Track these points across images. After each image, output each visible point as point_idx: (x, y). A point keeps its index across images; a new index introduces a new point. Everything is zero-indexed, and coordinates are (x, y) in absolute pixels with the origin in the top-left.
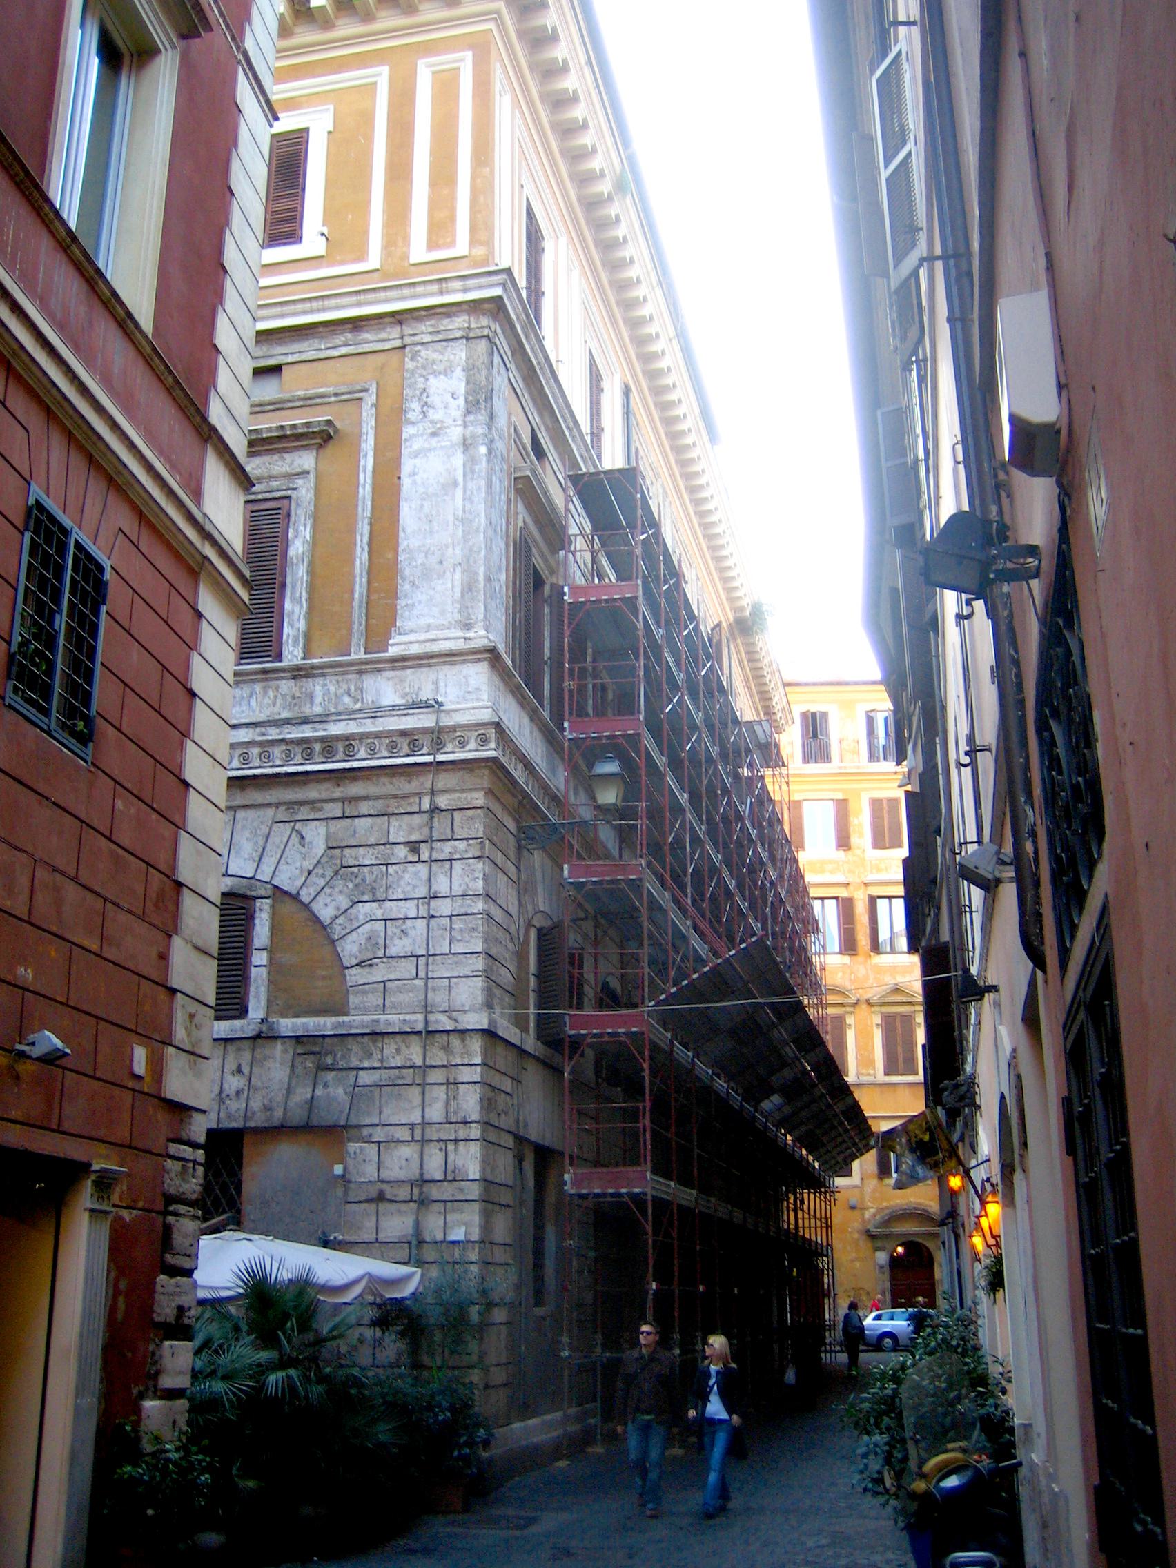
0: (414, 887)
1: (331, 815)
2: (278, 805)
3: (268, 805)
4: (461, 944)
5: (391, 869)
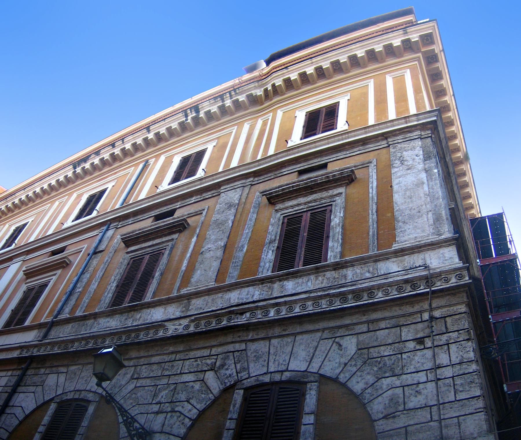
0: (423, 364)
1: (360, 331)
2: (323, 330)
3: (318, 330)
4: (464, 393)
5: (404, 356)
